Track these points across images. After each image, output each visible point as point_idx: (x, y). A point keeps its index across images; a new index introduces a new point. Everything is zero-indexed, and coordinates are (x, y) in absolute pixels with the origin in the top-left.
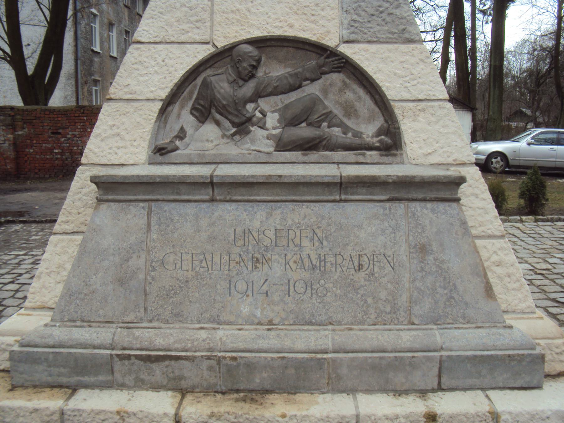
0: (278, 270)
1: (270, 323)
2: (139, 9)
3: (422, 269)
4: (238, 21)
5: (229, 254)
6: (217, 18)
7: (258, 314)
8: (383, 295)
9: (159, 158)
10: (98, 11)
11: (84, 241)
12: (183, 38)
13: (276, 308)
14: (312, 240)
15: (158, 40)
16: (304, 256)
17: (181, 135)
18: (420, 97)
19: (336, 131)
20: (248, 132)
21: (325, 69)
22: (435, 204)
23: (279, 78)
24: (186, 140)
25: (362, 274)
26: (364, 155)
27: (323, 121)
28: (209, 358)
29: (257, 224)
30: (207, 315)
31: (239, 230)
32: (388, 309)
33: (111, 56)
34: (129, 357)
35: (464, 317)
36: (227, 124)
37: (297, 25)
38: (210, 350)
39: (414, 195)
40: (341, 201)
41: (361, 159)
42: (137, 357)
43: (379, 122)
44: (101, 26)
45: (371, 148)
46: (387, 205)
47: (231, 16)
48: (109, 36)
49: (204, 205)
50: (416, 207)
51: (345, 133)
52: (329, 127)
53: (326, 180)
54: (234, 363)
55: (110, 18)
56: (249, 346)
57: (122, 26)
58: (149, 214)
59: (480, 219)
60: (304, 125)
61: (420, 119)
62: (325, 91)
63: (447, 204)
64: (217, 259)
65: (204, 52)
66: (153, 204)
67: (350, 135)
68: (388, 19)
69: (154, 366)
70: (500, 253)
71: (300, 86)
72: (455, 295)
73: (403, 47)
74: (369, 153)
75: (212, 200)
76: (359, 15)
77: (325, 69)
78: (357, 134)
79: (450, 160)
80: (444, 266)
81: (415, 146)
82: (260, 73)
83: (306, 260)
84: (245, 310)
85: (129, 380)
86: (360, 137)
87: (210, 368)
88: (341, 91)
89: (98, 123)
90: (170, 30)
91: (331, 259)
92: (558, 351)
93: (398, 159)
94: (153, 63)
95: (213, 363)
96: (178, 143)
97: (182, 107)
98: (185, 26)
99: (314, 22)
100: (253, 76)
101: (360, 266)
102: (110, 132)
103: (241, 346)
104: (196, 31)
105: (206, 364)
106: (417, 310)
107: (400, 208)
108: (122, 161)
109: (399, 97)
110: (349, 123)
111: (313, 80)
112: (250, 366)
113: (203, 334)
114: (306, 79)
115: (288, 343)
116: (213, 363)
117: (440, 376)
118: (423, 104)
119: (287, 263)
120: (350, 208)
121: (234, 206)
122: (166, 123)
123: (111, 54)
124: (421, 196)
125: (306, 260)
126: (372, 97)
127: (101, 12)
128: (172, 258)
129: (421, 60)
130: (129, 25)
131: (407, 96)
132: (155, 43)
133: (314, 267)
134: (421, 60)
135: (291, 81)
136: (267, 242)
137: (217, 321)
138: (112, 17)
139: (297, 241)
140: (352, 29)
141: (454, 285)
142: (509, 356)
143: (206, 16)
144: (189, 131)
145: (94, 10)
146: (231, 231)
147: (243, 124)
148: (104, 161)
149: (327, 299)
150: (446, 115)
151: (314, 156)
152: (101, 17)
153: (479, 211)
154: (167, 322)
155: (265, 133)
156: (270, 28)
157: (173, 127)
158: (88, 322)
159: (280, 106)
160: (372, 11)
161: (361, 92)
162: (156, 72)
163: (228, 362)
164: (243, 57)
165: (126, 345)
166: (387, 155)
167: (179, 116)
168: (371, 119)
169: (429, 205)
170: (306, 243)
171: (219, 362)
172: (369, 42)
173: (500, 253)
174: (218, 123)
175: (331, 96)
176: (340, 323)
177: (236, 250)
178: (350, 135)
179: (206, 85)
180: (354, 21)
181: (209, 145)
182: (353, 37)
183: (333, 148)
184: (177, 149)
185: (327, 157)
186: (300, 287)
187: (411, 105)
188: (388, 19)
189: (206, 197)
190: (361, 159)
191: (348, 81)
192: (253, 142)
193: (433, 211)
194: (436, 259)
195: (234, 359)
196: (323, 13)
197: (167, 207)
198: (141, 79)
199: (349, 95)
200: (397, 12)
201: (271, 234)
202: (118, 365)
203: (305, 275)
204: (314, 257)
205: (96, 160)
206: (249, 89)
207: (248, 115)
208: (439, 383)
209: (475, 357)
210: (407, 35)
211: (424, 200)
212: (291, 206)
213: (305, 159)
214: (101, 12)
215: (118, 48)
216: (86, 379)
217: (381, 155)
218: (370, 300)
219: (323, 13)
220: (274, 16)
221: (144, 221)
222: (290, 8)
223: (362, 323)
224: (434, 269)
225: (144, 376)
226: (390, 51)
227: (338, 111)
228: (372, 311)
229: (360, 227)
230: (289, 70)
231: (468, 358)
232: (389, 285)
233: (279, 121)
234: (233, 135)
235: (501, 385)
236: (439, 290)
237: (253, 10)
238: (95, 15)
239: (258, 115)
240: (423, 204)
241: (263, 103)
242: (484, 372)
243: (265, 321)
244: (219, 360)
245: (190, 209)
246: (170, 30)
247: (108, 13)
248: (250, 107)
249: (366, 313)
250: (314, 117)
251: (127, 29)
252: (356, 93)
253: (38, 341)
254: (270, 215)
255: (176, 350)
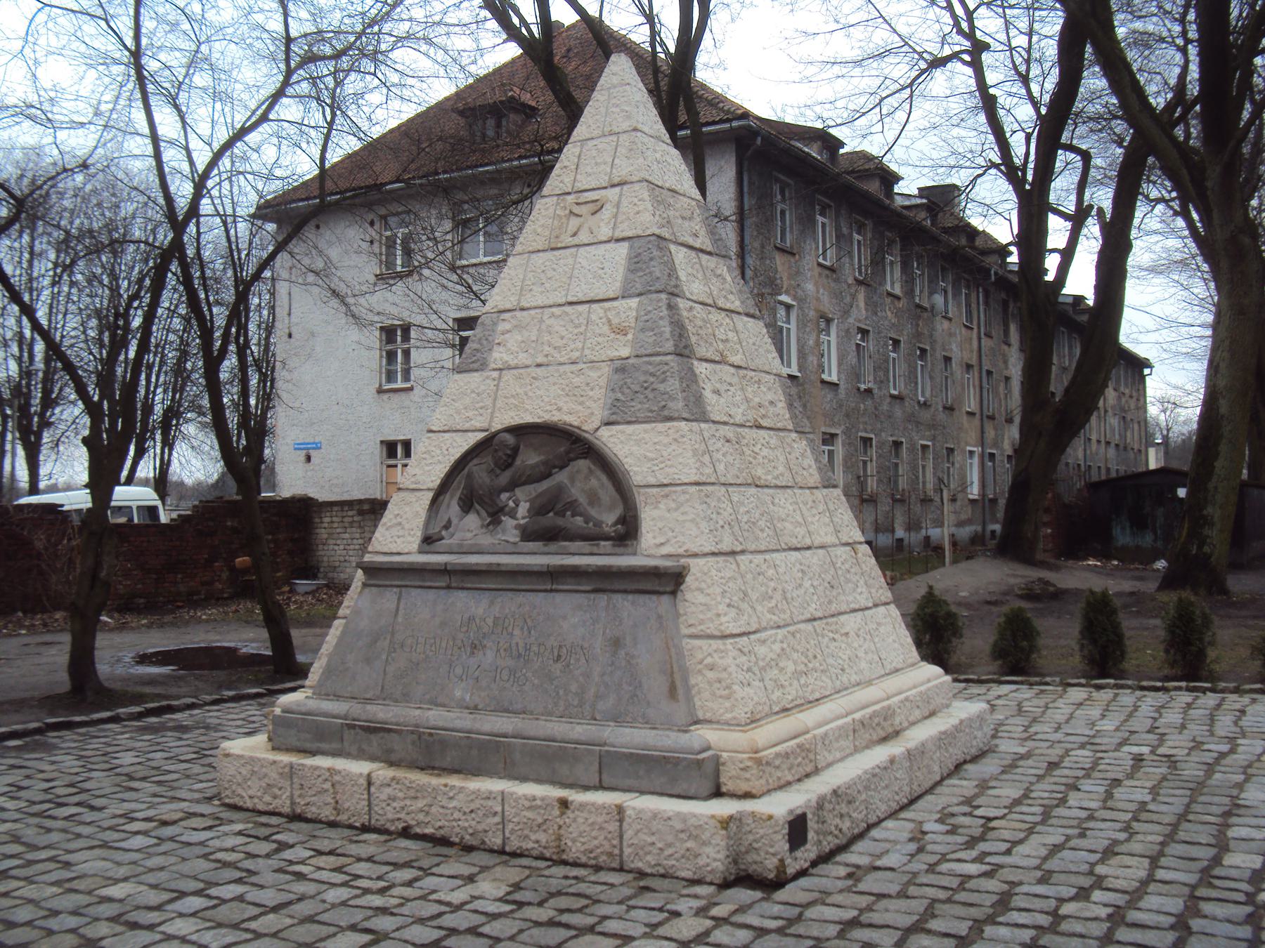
0: (490, 655)
1: (476, 708)
2: (893, 284)
3: (613, 663)
4: (516, 406)
5: (454, 639)
6: (499, 403)
7: (468, 698)
8: (574, 687)
9: (427, 548)
10: (795, 298)
11: (346, 624)
12: (467, 426)
13: (483, 694)
14: (522, 629)
15: (446, 428)
16: (513, 645)
17: (447, 526)
18: (665, 482)
19: (579, 520)
20: (500, 522)
21: (572, 455)
22: (636, 596)
23: (533, 467)
24: (451, 530)
25: (559, 665)
26: (598, 545)
27: (566, 510)
28: (412, 732)
29: (480, 611)
30: (428, 697)
31: (466, 616)
32: (576, 703)
33: (823, 382)
34: (353, 727)
35: (644, 716)
36: (484, 514)
37: (565, 408)
38: (417, 726)
39: (617, 586)
40: (551, 591)
41: (595, 550)
42: (360, 727)
43: (618, 512)
44: (802, 325)
45: (607, 538)
46: (592, 596)
47: (512, 400)
48: (818, 343)
49: (442, 592)
50: (618, 598)
51: (587, 523)
52: (573, 516)
53: (536, 569)
54: (431, 739)
55: (821, 308)
56: (451, 725)
57: (851, 320)
58: (399, 599)
59: (701, 616)
60: (551, 514)
61: (662, 506)
62: (572, 479)
63: (647, 596)
64: (444, 645)
65: (481, 435)
66: (404, 590)
67: (591, 524)
68: (651, 396)
69: (372, 736)
70: (715, 655)
71: (549, 475)
72: (638, 693)
73: (660, 426)
74: (603, 543)
75: (448, 587)
76: (623, 393)
77: (572, 455)
78: (598, 524)
79: (681, 551)
80: (633, 662)
81: (650, 535)
82: (518, 462)
83: (514, 648)
84: (458, 694)
85: (354, 750)
86: (600, 527)
87: (413, 743)
88: (587, 478)
89: (387, 512)
90: (457, 418)
91: (535, 648)
92: (741, 766)
93: (630, 550)
94: (438, 452)
95: (415, 737)
96: (444, 533)
97: (452, 497)
98: (470, 414)
99: (581, 403)
100: (509, 465)
101: (559, 656)
102: (394, 521)
103: (441, 724)
104: (479, 418)
105: (410, 738)
106: (601, 706)
107: (602, 599)
108: (399, 550)
109: (644, 483)
110: (593, 512)
111: (562, 468)
112: (444, 744)
113: (417, 712)
114: (555, 467)
115: (477, 726)
116: (415, 737)
117: (600, 773)
118: (667, 490)
119: (498, 651)
120: (559, 598)
121: (465, 592)
122: (437, 513)
123: (825, 377)
124: (622, 587)
125: (514, 648)
126: (614, 485)
127: (801, 301)
128: (409, 641)
129: (675, 440)
130: (866, 318)
131: (652, 481)
132: (444, 432)
133: (519, 656)
134: (675, 440)
135: (542, 468)
136: (486, 630)
137: (435, 703)
138: (827, 304)
139: (510, 629)
140: (615, 409)
141: (640, 682)
142: (664, 757)
143: (489, 402)
144: (455, 521)
145: (784, 298)
146: (459, 618)
147: (496, 513)
148: (386, 550)
149: (526, 688)
150: (688, 501)
151: (553, 547)
152: (800, 308)
153: (701, 608)
154: (396, 701)
155: (515, 522)
156: (541, 413)
157: (443, 518)
158: (338, 697)
159: (534, 494)
160: (637, 388)
161: (604, 478)
162: (440, 462)
163: (426, 737)
164: (504, 444)
165: (356, 716)
166: (619, 546)
167: (448, 506)
168: (611, 508)
169: (630, 597)
170: (517, 632)
171: (420, 738)
172: (629, 423)
173: (715, 655)
174: (478, 513)
175: (578, 484)
176: (532, 714)
177: (461, 636)
178: (591, 524)
179: (470, 476)
180: (618, 400)
181: (469, 535)
182: (614, 418)
183: (572, 538)
184: (442, 538)
185: (565, 547)
186: (505, 673)
187: (655, 490)
188: (651, 396)
189: (444, 584)
190: (595, 550)
191: (593, 467)
192: (504, 531)
193: (633, 603)
194: (627, 654)
195: (431, 735)
196: (591, 393)
197: (414, 592)
198: (427, 468)
199: (594, 482)
200: (661, 387)
201: (490, 621)
202: (348, 735)
203: (510, 662)
204: (521, 645)
205: (379, 548)
206: (505, 478)
207: (501, 505)
208: (600, 780)
209: (632, 754)
210: (666, 413)
211: (625, 592)
212: (510, 594)
213: (546, 549)
214: (801, 301)
215: (840, 365)
216: (324, 746)
217: (614, 546)
218: (561, 692)
219: (591, 393)
220: (546, 399)
221: (394, 606)
222: (563, 390)
223: (550, 714)
224: (623, 663)
225: (365, 746)
226: (646, 431)
227: (582, 500)
228: (562, 703)
229: (565, 618)
230: (542, 457)
231: (624, 754)
232: (581, 679)
233: (529, 511)
234: (488, 525)
235: (658, 790)
236: (625, 686)
237: (530, 394)
238: (788, 307)
239: (511, 504)
240: (624, 596)
241: (519, 492)
242: (641, 773)
243: (472, 705)
244: (420, 735)
245: (431, 594)
246: (457, 418)
247: (818, 299)
248: (504, 496)
249: (556, 704)
250: (559, 506)
251: (863, 326)
252: (599, 480)
253: (295, 708)
254: (492, 603)
255: (391, 724)
